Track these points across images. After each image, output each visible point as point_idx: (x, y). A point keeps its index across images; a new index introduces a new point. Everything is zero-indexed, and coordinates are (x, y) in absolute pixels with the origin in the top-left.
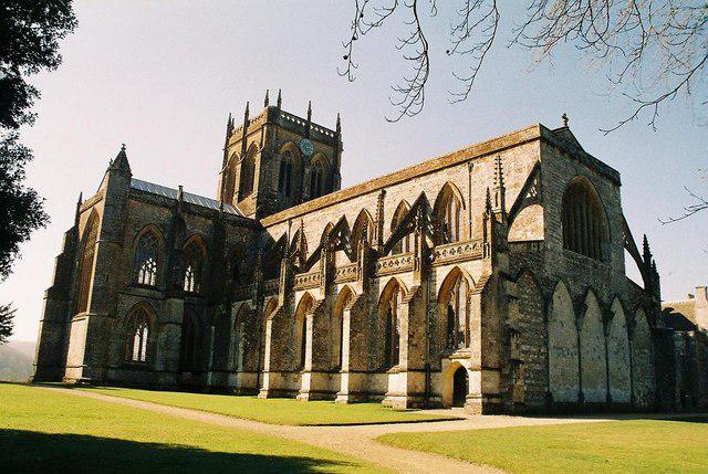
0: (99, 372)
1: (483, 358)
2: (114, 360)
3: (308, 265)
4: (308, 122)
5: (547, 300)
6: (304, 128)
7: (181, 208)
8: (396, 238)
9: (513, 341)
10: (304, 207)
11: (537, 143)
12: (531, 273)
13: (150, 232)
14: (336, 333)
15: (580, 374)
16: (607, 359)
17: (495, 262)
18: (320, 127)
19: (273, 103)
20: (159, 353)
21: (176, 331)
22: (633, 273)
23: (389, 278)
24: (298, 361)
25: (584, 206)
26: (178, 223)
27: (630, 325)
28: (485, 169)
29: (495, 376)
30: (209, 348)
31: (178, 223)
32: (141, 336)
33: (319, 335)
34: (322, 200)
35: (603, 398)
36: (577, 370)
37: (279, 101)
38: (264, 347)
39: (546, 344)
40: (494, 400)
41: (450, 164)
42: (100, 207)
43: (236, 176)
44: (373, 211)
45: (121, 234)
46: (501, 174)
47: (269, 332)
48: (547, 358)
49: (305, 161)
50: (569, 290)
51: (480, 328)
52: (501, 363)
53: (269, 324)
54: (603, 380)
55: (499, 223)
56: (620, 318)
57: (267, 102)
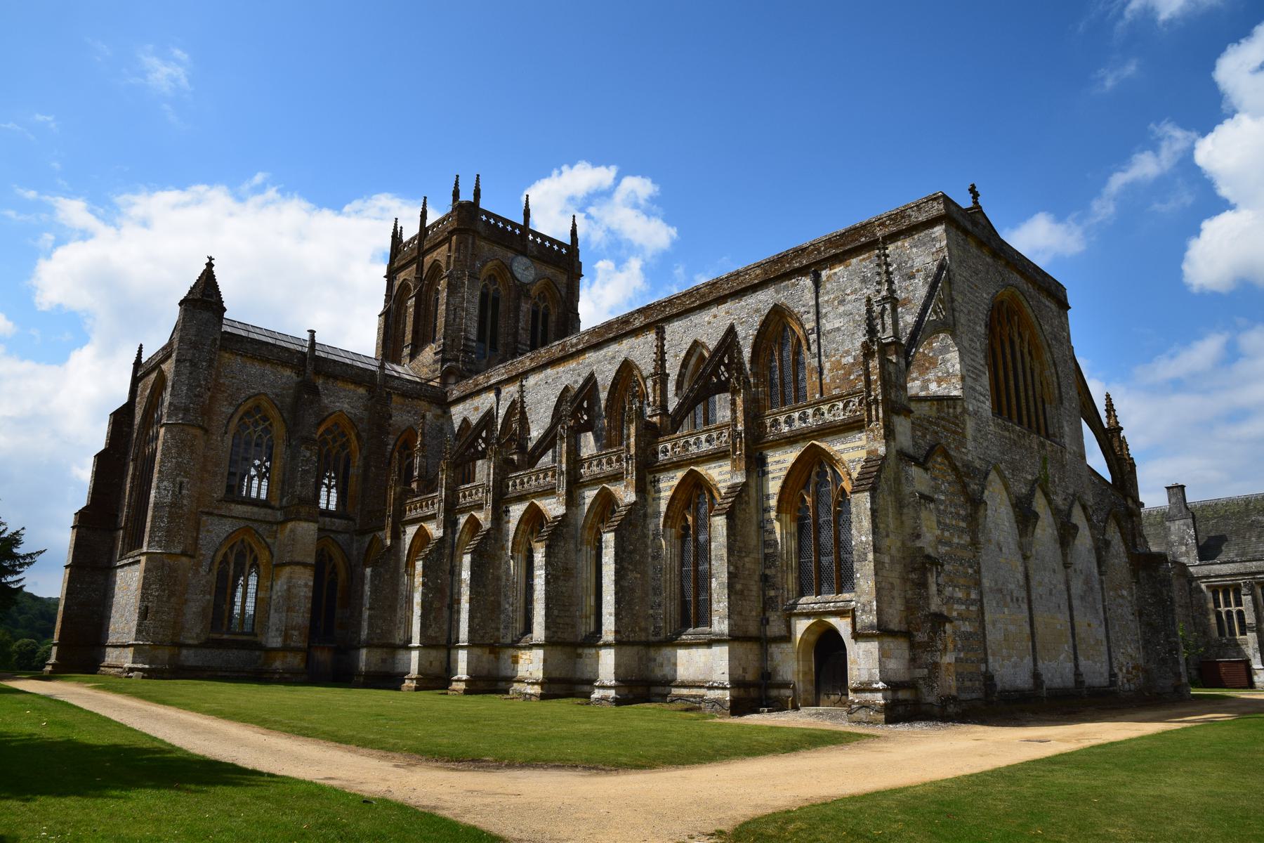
0: (164, 654)
1: (880, 612)
2: (194, 630)
3: (531, 458)
4: (525, 229)
5: (976, 503)
6: (517, 237)
7: (311, 366)
8: (687, 407)
9: (932, 579)
10: (526, 362)
11: (939, 230)
12: (946, 455)
13: (258, 408)
14: (587, 573)
15: (1033, 634)
16: (1071, 608)
17: (889, 434)
18: (552, 241)
19: (466, 196)
20: (274, 618)
21: (304, 580)
22: (1096, 460)
23: (680, 474)
24: (519, 625)
25: (1017, 340)
26: (307, 390)
27: (1101, 548)
28: (849, 284)
29: (900, 648)
30: (362, 605)
31: (307, 390)
32: (246, 586)
33: (556, 578)
34: (555, 348)
35: (1070, 682)
36: (1027, 629)
37: (477, 194)
38: (459, 602)
39: (978, 584)
40: (902, 695)
41: (779, 271)
42: (169, 367)
43: (403, 320)
44: (646, 365)
45: (207, 411)
46: (888, 273)
47: (466, 575)
48: (981, 611)
49: (521, 290)
50: (1007, 488)
51: (871, 556)
52: (910, 628)
53: (467, 559)
54: (1067, 647)
55: (891, 355)
56: (1084, 540)
57: (456, 194)
